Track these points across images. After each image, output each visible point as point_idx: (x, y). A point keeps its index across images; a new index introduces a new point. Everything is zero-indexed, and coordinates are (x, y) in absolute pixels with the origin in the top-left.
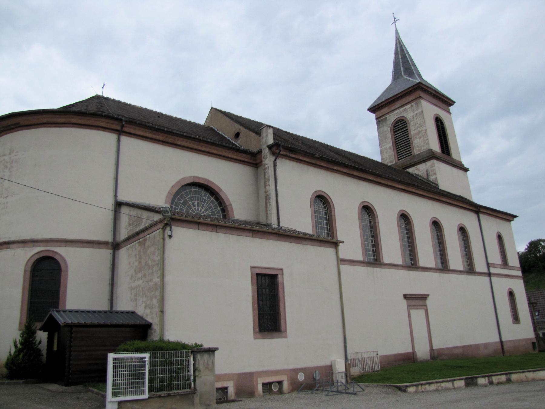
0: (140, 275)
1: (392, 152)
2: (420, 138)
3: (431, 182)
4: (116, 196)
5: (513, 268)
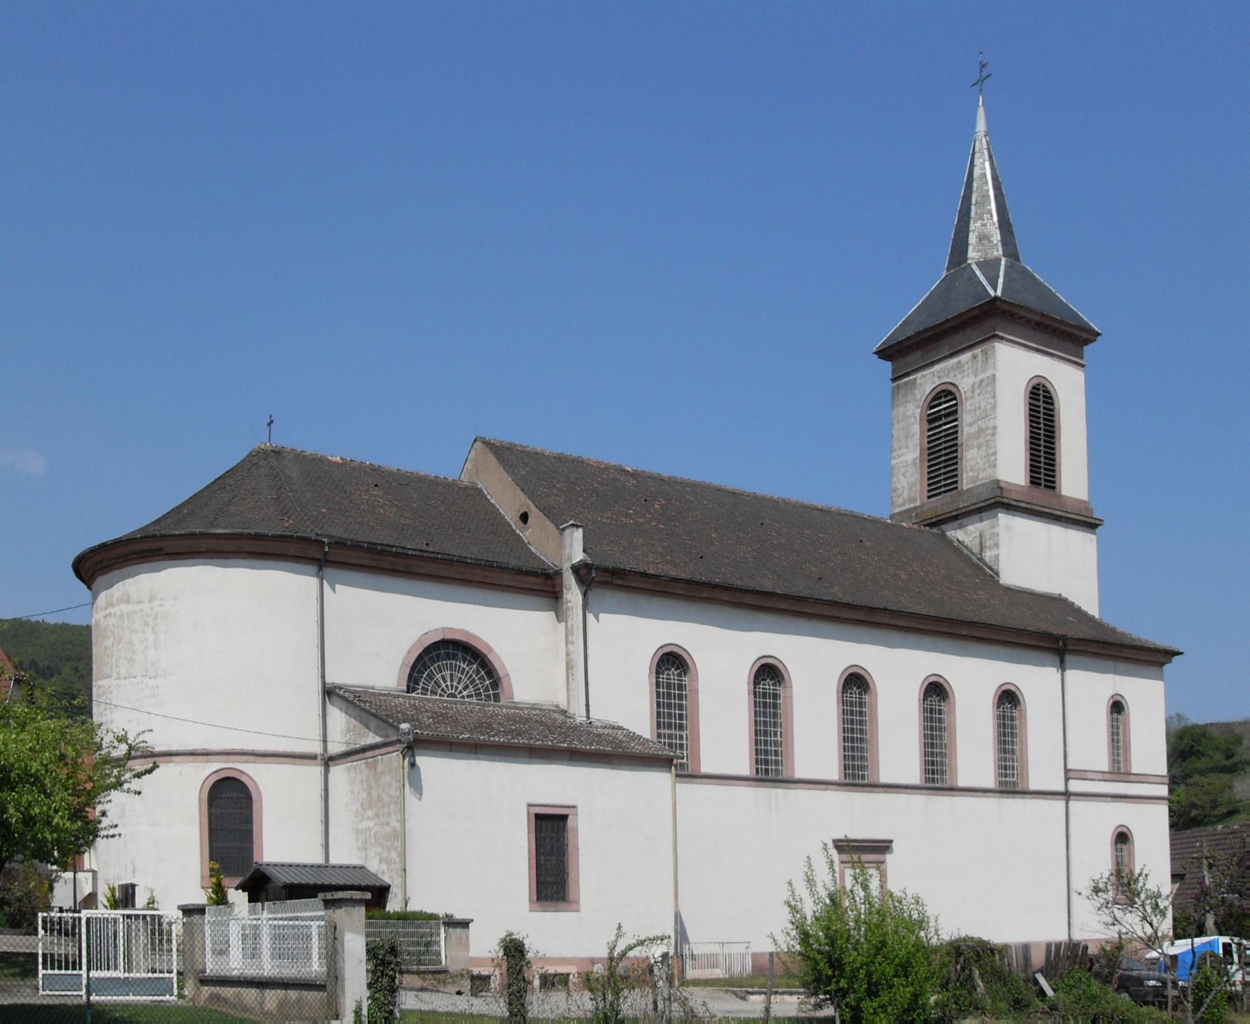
0: (370, 813)
1: (917, 475)
2: (979, 447)
3: (986, 564)
4: (323, 677)
5: (1142, 778)
